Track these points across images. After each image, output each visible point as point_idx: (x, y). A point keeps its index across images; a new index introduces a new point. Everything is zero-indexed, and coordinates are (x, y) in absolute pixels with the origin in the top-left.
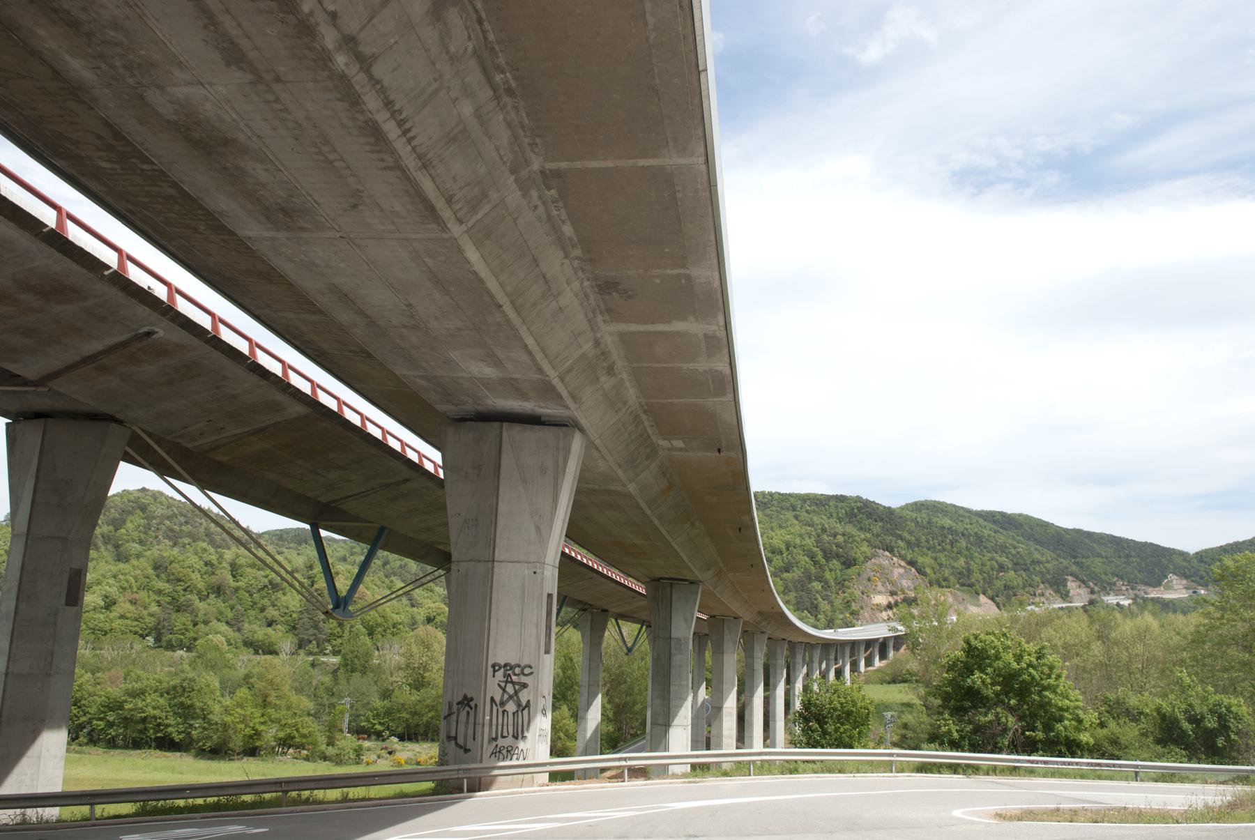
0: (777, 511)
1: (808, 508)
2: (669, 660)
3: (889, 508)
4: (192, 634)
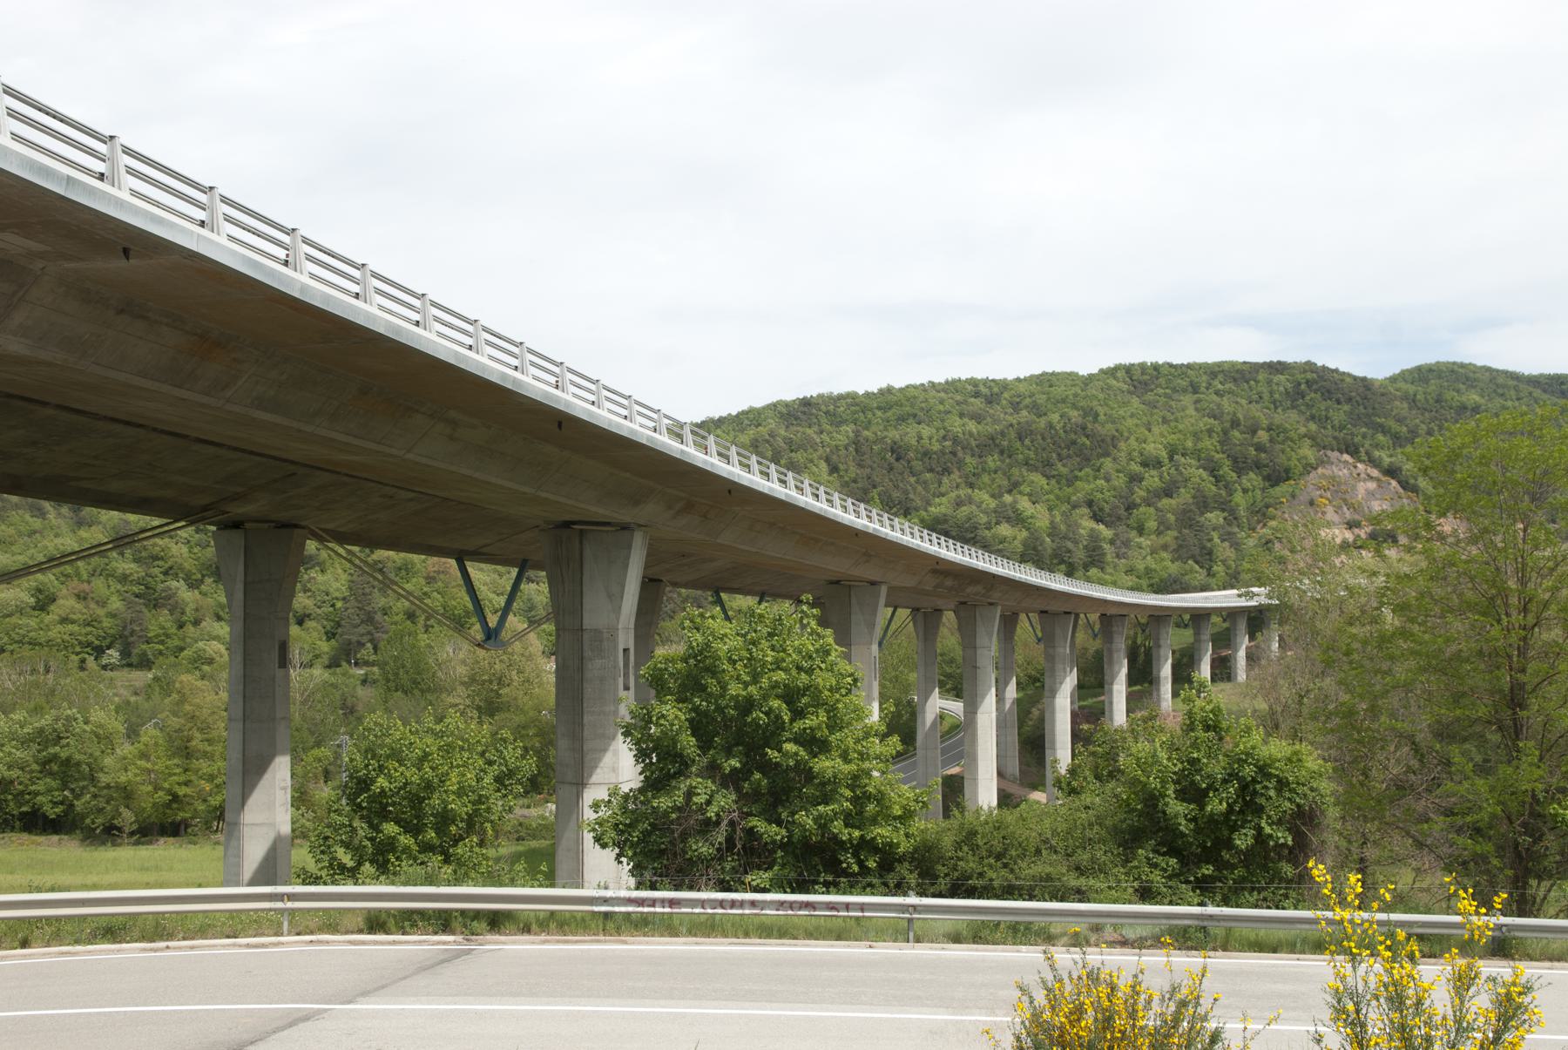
0: (1166, 395)
1: (1220, 386)
2: (581, 669)
3: (1364, 379)
4: (177, 642)
